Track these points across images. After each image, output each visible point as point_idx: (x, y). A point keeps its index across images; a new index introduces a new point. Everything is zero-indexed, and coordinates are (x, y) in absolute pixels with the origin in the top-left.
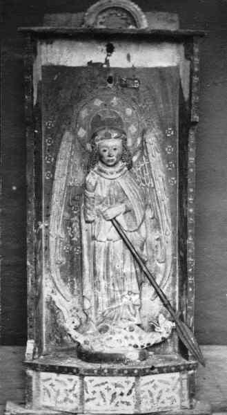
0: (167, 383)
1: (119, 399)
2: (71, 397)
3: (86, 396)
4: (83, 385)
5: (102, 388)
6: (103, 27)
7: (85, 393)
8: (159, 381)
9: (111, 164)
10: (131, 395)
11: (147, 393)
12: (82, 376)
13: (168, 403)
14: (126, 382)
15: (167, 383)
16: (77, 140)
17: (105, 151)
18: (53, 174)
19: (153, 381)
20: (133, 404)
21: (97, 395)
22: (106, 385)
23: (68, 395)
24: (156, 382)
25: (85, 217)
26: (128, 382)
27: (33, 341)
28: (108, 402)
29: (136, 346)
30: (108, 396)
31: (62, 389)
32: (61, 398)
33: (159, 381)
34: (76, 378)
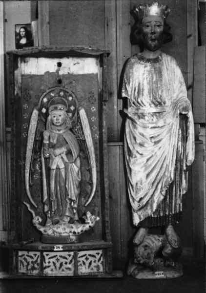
0: (64, 258)
1: (64, 266)
2: (36, 266)
3: (45, 265)
4: (43, 258)
5: (54, 260)
6: (106, 61)
7: (44, 263)
8: (60, 256)
9: (58, 124)
10: (72, 264)
11: (81, 263)
12: (42, 252)
13: (95, 270)
14: (68, 255)
15: (64, 258)
16: (41, 115)
17: (54, 117)
18: (27, 134)
19: (24, 255)
20: (73, 269)
21: (51, 264)
22: (57, 257)
23: (34, 265)
24: (58, 257)
25: (44, 155)
26: (98, 254)
27: (144, 230)
28: (87, 267)
29: (74, 233)
30: (58, 265)
31: (30, 260)
32: (29, 267)
33: (60, 256)
34: (38, 253)
